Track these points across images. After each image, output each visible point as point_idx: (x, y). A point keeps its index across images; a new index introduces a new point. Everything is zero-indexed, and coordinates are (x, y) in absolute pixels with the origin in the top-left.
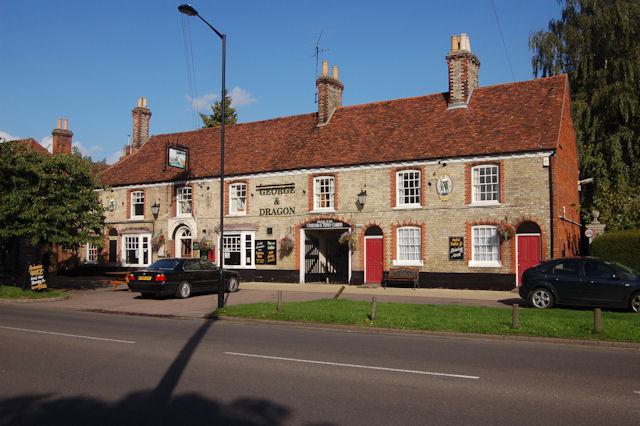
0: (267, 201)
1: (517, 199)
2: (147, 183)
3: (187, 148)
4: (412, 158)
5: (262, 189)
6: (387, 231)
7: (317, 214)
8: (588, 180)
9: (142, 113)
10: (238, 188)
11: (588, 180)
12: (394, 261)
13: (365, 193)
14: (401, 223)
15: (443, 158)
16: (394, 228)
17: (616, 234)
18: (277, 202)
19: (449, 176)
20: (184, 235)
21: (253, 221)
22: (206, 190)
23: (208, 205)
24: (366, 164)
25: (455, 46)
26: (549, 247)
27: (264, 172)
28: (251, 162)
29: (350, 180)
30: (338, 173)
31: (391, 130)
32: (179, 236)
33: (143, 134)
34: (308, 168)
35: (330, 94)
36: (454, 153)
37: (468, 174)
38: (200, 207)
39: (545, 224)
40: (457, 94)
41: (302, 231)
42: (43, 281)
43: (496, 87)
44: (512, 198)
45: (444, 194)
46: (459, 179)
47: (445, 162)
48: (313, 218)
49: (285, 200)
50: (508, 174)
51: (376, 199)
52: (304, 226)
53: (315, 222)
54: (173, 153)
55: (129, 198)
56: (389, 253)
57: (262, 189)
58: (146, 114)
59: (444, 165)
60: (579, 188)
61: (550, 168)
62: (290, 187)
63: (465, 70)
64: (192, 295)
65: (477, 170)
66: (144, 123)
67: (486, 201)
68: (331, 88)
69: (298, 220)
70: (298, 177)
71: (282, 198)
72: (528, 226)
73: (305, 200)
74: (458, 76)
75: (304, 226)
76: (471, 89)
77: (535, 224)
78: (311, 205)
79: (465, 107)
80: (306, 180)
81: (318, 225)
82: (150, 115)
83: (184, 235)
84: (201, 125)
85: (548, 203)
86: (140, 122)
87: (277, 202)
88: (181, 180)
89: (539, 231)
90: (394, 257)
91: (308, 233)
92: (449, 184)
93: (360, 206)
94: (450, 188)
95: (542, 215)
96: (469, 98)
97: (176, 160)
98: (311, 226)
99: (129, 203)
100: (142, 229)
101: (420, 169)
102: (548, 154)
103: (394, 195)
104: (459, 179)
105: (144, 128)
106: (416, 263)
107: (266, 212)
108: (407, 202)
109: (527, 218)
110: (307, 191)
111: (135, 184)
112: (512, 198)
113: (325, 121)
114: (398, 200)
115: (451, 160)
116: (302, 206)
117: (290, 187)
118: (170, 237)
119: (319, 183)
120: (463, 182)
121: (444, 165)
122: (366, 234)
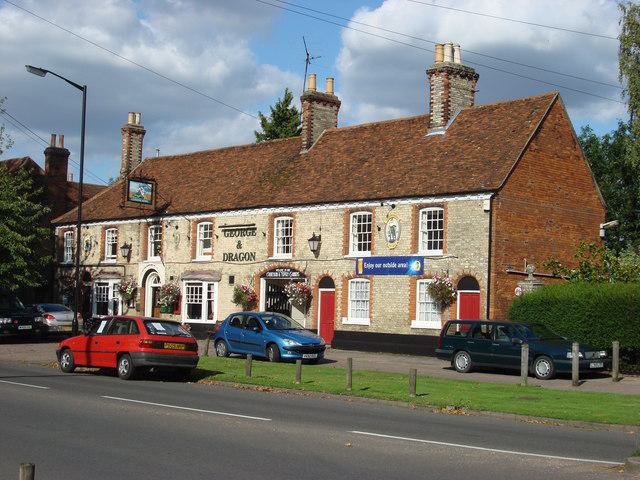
0: (227, 244)
1: (458, 249)
2: (121, 219)
3: (153, 180)
4: (362, 197)
5: (229, 231)
6: (338, 283)
7: (276, 261)
8: (612, 223)
9: (136, 132)
10: (206, 228)
11: (612, 223)
12: (344, 319)
13: (321, 238)
14: (351, 274)
15: (392, 198)
16: (346, 279)
17: (563, 289)
18: (239, 246)
19: (398, 223)
20: (155, 282)
21: (216, 267)
22: (178, 227)
23: (177, 247)
24: (321, 203)
25: (439, 58)
26: (486, 307)
27: (229, 210)
28: (222, 197)
29: (309, 219)
30: (296, 213)
31: (363, 161)
32: (150, 284)
33: (135, 157)
34: (269, 207)
35: (317, 114)
36: (403, 193)
37: (416, 218)
38: (168, 249)
39: (483, 279)
40: (437, 119)
41: (263, 282)
42: (212, 343)
43: (196, 153)
44: (453, 248)
45: (392, 242)
46: (406, 224)
47: (395, 203)
48: (272, 265)
49: (249, 244)
50: (450, 220)
51: (331, 244)
52: (263, 275)
53: (274, 270)
54: (134, 187)
55: (103, 236)
56: (339, 309)
57: (229, 231)
58: (138, 133)
59: (393, 206)
60: (602, 233)
61: (490, 211)
62: (250, 229)
63: (447, 86)
64: (472, 370)
65: (355, 216)
66: (136, 143)
67: (433, 250)
68: (320, 106)
69: (258, 268)
70: (259, 217)
71: (244, 240)
72: (468, 282)
73: (264, 245)
74: (439, 94)
75: (263, 275)
76: (456, 110)
77: (474, 279)
78: (271, 251)
79: (443, 133)
80: (267, 220)
81: (276, 274)
82: (143, 133)
83: (155, 282)
84: (253, 140)
85: (486, 255)
86: (130, 143)
87: (239, 246)
88: (157, 213)
89: (333, 286)
90: (345, 314)
91: (269, 283)
92: (397, 229)
93: (316, 252)
94: (397, 234)
95: (480, 267)
96: (451, 122)
97: (139, 193)
98: (270, 274)
99: (195, 238)
100: (114, 273)
101: (442, 206)
102: (489, 196)
103: (347, 241)
104: (406, 224)
105: (135, 150)
106: (366, 321)
107: (229, 257)
108: (430, 248)
109: (467, 272)
110: (99, 243)
111: (109, 220)
112: (453, 248)
113: (308, 146)
114: (420, 245)
115: (399, 201)
116: (263, 252)
117: (250, 229)
118: (140, 285)
119: (426, 216)
120: (410, 228)
121: (393, 206)
122: (321, 287)
